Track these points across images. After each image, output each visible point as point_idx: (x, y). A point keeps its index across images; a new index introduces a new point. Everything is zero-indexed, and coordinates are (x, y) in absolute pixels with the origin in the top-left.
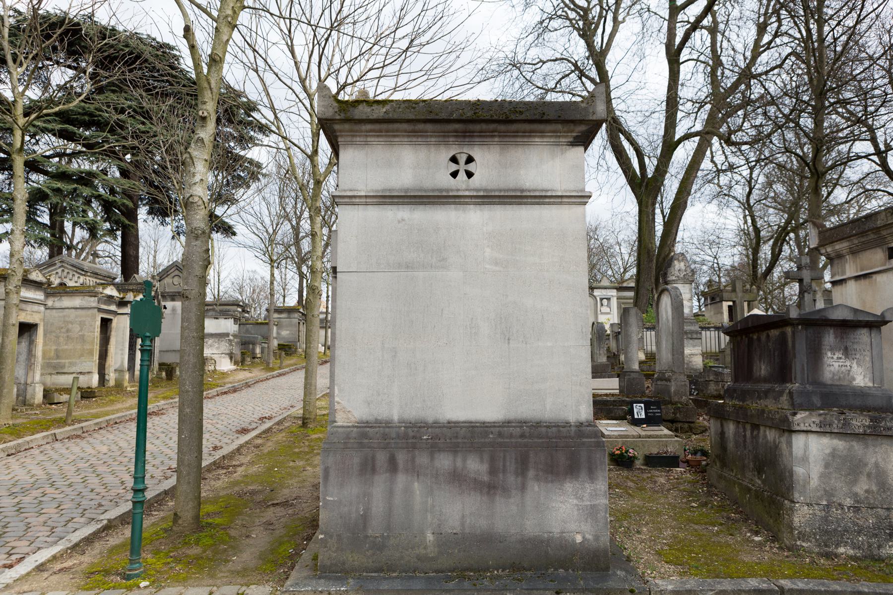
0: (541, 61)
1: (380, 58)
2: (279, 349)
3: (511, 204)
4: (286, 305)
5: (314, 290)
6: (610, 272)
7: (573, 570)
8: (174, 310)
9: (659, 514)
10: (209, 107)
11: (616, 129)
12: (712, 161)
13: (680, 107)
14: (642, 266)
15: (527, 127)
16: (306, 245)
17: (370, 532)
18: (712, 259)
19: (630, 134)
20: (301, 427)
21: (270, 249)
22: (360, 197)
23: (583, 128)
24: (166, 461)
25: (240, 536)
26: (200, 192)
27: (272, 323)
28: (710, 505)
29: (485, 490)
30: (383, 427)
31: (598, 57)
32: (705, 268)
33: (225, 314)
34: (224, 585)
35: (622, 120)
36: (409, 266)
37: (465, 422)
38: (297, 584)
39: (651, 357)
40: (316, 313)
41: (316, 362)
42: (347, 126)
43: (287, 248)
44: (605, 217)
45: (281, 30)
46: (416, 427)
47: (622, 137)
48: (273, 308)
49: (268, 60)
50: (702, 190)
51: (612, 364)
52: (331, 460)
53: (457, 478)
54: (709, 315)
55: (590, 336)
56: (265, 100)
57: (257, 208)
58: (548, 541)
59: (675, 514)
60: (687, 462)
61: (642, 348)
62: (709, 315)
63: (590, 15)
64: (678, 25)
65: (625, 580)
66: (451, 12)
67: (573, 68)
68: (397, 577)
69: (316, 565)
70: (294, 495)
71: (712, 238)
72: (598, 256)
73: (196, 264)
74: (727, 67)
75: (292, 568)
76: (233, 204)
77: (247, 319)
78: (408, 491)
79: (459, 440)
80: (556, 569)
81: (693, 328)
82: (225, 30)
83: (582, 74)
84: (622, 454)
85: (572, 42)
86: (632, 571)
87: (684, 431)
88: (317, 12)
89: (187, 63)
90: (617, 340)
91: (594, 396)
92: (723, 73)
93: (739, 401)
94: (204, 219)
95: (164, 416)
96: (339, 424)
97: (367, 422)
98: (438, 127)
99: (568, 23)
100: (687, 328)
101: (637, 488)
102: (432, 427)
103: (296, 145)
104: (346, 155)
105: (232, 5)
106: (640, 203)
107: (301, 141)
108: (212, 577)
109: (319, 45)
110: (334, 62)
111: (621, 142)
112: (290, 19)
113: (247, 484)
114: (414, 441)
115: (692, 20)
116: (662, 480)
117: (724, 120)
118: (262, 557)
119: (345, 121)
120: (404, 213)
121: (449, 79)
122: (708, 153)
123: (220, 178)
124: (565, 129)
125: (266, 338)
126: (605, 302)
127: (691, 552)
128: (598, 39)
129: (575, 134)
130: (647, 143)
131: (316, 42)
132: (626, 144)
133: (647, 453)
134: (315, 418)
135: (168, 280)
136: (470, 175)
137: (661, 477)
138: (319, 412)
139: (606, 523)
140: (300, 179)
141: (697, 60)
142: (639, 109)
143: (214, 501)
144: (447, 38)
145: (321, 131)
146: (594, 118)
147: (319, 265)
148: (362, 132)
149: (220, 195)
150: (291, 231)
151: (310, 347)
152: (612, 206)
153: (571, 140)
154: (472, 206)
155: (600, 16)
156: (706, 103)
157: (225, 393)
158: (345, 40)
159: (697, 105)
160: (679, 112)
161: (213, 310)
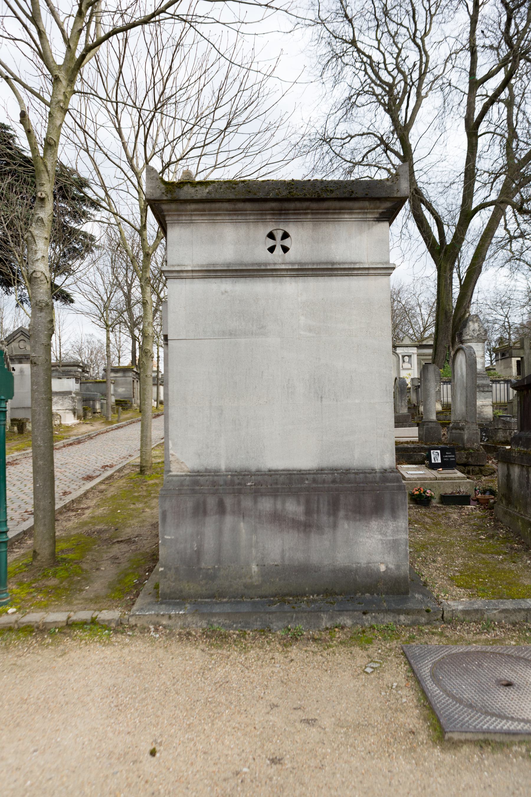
0: (349, 136)
1: (202, 137)
2: (117, 405)
3: (323, 276)
4: (121, 365)
5: (146, 353)
6: (411, 332)
7: (378, 594)
8: (22, 371)
9: (452, 545)
10: (47, 188)
11: (418, 198)
12: (505, 228)
13: (477, 178)
14: (440, 326)
15: (337, 204)
16: (137, 311)
17: (203, 565)
18: (503, 318)
19: (431, 204)
20: (139, 474)
21: (105, 315)
22: (187, 271)
23: (388, 205)
24: (23, 505)
25: (91, 569)
26: (42, 268)
27: (109, 382)
28: (496, 537)
29: (302, 528)
30: (213, 476)
31: (402, 131)
32: (497, 326)
33: (67, 375)
34: (79, 610)
35: (424, 192)
36: (232, 334)
37: (284, 470)
38: (142, 609)
39: (447, 408)
40: (149, 373)
41: (150, 417)
42: (173, 206)
43: (121, 313)
44: (407, 281)
45: (108, 111)
46: (241, 475)
47: (423, 206)
48: (110, 368)
49: (98, 141)
50: (496, 255)
51: (413, 414)
52: (167, 505)
53: (277, 518)
54: (500, 370)
55: (393, 390)
56: (97, 179)
57: (92, 278)
58: (356, 570)
59: (466, 545)
60: (477, 500)
61: (439, 400)
62: (500, 370)
63: (395, 91)
64: (477, 99)
65: (421, 602)
66: (266, 92)
67: (379, 142)
68: (227, 602)
69: (158, 593)
70: (136, 533)
71: (504, 299)
72: (400, 316)
73: (42, 330)
74: (522, 139)
75: (137, 595)
76: (70, 274)
77: (87, 378)
78: (235, 530)
79: (279, 486)
80: (363, 594)
81: (485, 382)
82: (58, 114)
83: (387, 148)
84: (420, 494)
85: (378, 117)
86: (428, 594)
87: (474, 473)
88: (141, 94)
89: (22, 142)
90: (417, 393)
91: (397, 443)
92: (518, 145)
93: (524, 447)
94: (47, 292)
95: (18, 466)
96: (173, 473)
97: (198, 472)
98: (256, 206)
99: (374, 99)
100: (479, 382)
101: (433, 524)
102: (255, 475)
103: (126, 221)
104: (173, 232)
105: (63, 90)
106: (439, 269)
107: (131, 216)
108: (69, 603)
109: (144, 125)
110: (158, 142)
111: (422, 212)
112: (117, 103)
113: (94, 524)
114: (239, 487)
115: (490, 93)
116: (455, 516)
117: (517, 190)
118: (111, 587)
119: (173, 201)
120: (227, 286)
121: (266, 155)
122: (502, 221)
123: (57, 250)
124: (372, 206)
125: (105, 395)
126: (406, 359)
127: (478, 577)
128: (402, 114)
129: (380, 211)
130: (446, 212)
131: (141, 123)
132: (427, 214)
133: (442, 493)
134: (151, 467)
135: (14, 345)
136: (285, 249)
137: (454, 513)
138: (155, 461)
139: (406, 555)
140: (130, 252)
141: (494, 133)
142: (440, 180)
143: (67, 539)
144: (262, 118)
145: (149, 207)
146: (399, 195)
147: (150, 330)
148: (186, 211)
149: (58, 267)
150: (123, 298)
151: (144, 404)
152: (414, 271)
153: (377, 216)
154: (288, 279)
155: (405, 92)
156: (501, 174)
157: (71, 444)
158: (168, 121)
159: (493, 176)
160: (476, 183)
161: (57, 370)
